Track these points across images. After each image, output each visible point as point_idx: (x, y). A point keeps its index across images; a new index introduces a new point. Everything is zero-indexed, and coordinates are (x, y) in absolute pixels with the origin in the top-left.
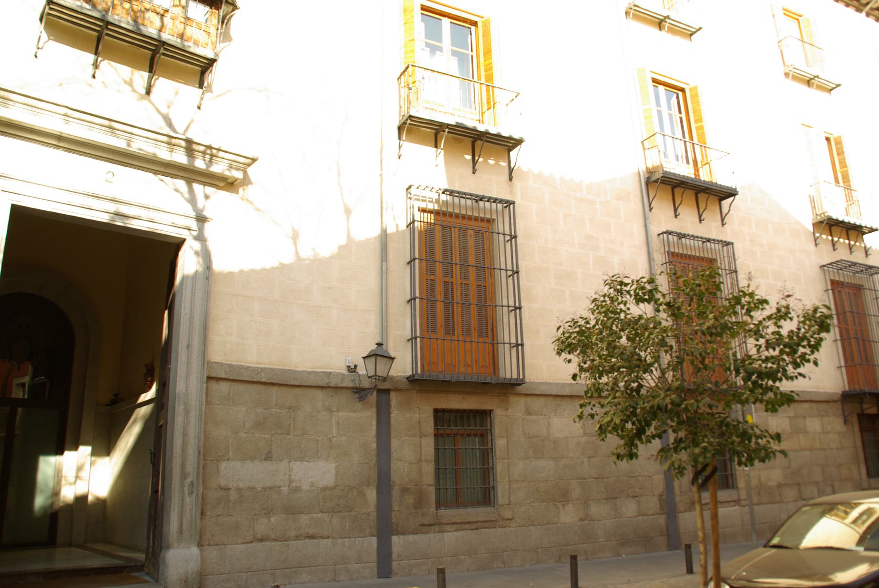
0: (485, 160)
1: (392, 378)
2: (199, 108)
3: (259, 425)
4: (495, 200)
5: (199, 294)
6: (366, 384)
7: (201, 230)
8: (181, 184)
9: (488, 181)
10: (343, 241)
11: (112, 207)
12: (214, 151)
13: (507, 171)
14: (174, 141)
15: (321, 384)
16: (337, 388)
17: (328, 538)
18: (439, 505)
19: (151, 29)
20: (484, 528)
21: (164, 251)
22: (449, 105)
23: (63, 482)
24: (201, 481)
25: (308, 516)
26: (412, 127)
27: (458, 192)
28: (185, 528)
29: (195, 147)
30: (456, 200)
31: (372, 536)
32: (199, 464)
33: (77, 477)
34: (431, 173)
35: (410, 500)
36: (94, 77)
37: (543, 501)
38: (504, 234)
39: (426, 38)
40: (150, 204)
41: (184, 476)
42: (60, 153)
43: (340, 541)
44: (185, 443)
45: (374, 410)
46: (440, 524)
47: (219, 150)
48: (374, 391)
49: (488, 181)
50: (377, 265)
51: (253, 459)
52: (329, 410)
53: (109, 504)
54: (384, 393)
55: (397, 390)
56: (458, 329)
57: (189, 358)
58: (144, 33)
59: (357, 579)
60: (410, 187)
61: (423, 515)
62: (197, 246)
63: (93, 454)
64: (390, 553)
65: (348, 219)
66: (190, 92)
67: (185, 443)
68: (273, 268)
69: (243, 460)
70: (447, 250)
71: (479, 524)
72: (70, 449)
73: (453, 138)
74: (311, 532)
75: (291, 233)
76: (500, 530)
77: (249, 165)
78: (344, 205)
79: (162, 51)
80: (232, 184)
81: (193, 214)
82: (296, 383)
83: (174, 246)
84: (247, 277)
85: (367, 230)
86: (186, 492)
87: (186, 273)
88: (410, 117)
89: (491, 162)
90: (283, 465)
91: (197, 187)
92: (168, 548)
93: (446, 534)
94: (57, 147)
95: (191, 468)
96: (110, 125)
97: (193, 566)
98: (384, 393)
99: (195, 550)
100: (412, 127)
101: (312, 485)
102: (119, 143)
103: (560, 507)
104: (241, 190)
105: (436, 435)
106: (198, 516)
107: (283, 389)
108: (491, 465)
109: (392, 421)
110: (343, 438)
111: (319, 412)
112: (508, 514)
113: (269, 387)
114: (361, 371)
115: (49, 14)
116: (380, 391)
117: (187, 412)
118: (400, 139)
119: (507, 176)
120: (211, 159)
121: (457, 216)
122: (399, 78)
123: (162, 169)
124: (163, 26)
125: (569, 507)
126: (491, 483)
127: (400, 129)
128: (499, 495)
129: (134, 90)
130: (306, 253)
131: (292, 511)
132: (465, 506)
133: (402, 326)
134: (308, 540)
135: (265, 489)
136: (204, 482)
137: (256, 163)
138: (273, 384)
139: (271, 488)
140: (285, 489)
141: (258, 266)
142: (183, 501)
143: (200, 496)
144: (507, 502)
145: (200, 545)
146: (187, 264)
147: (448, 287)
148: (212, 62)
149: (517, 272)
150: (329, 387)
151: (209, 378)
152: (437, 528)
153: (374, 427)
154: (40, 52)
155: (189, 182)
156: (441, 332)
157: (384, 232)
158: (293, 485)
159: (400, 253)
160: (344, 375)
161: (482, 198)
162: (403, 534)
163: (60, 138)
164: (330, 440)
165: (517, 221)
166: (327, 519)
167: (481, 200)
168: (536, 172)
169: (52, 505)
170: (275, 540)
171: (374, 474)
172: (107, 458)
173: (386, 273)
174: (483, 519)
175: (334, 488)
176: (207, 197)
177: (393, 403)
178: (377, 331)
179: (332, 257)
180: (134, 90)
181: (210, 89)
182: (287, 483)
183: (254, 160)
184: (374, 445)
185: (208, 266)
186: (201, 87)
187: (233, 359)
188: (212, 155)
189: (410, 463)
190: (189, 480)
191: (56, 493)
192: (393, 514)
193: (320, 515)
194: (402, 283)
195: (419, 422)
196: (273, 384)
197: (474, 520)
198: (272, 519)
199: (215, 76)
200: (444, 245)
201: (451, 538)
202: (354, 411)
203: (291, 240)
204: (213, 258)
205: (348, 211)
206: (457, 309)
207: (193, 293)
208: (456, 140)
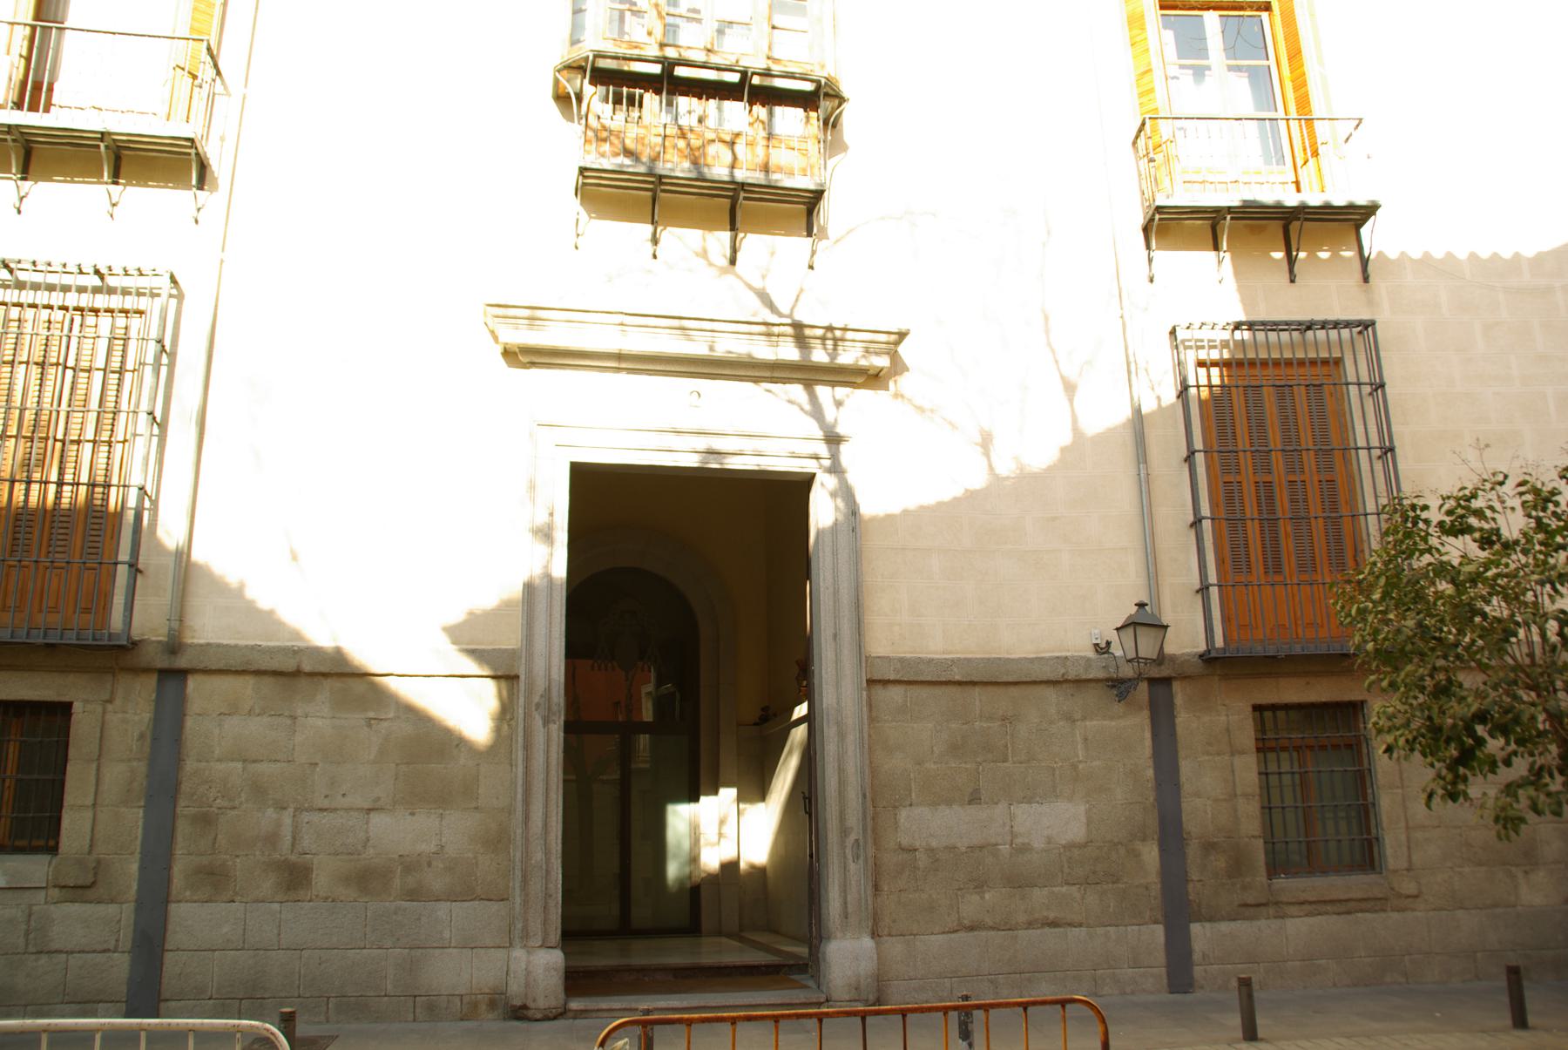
0: (1312, 254)
1: (1173, 658)
2: (811, 267)
3: (956, 748)
4: (1336, 325)
5: (844, 555)
6: (1128, 671)
7: (835, 457)
8: (797, 391)
9: (1323, 290)
10: (1066, 438)
11: (702, 443)
12: (838, 334)
13: (1357, 265)
14: (776, 330)
15: (1052, 677)
16: (1079, 682)
17: (1080, 925)
18: (1273, 870)
19: (719, 170)
20: (1362, 911)
21: (785, 495)
22: (1233, 166)
23: (702, 842)
24: (870, 841)
25: (1045, 891)
26: (1166, 225)
27: (1263, 323)
28: (850, 909)
29: (808, 332)
30: (1261, 336)
31: (1156, 922)
32: (864, 813)
33: (720, 835)
34: (1211, 296)
35: (1219, 862)
36: (655, 257)
37: (1480, 864)
38: (1359, 384)
39: (1228, 58)
40: (756, 430)
41: (844, 832)
42: (623, 377)
43: (1100, 931)
44: (842, 783)
45: (1146, 713)
46: (1276, 903)
47: (845, 329)
48: (1141, 681)
49: (1323, 290)
50: (1131, 470)
51: (949, 802)
52: (1071, 720)
53: (770, 872)
54: (1161, 684)
55: (1184, 678)
56: (1289, 563)
57: (838, 654)
58: (709, 176)
59: (1133, 993)
60: (1173, 332)
61: (1244, 888)
62: (831, 482)
63: (741, 798)
64: (1189, 952)
65: (1071, 401)
66: (796, 245)
67: (842, 783)
68: (955, 499)
69: (934, 804)
70: (1258, 426)
71: (1351, 905)
72: (707, 794)
73: (1246, 226)
74: (1052, 915)
75: (979, 440)
76: (1395, 915)
77: (897, 343)
78: (1062, 377)
79: (742, 195)
80: (877, 376)
81: (820, 434)
82: (1010, 679)
83: (800, 486)
84: (914, 519)
85: (1106, 412)
86: (850, 857)
87: (821, 526)
88: (1159, 209)
89: (1324, 255)
90: (1000, 810)
91: (823, 392)
92: (829, 938)
93: (1289, 922)
94: (619, 370)
95: (853, 820)
96: (680, 324)
97: (867, 966)
98: (1161, 684)
99: (867, 942)
100: (1166, 225)
101: (1049, 840)
102: (698, 348)
103: (1520, 875)
104: (891, 384)
105: (1258, 750)
106: (870, 891)
107: (991, 689)
108: (1370, 798)
109: (1179, 730)
110: (1097, 763)
111: (1052, 722)
112: (1409, 887)
113: (969, 689)
114: (1117, 651)
115: (584, 184)
116: (1152, 681)
117: (842, 736)
118: (1148, 247)
119: (1358, 275)
120: (835, 345)
121: (1264, 363)
122: (1134, 143)
123: (768, 374)
124: (735, 158)
125: (1540, 876)
126: (1374, 831)
127: (1146, 230)
128: (1389, 851)
129: (711, 264)
130: (1005, 468)
131: (1018, 882)
132: (1324, 872)
133: (1183, 567)
134: (1047, 930)
135: (972, 848)
136: (876, 842)
137: (907, 340)
138: (973, 683)
139: (981, 847)
140: (1005, 849)
141: (930, 500)
142: (845, 868)
143: (871, 862)
144: (1405, 865)
145: (875, 934)
146: (822, 512)
147: (1266, 492)
148: (818, 195)
149: (1392, 449)
150: (1067, 681)
151: (871, 682)
152: (1271, 911)
153: (1148, 742)
154: (580, 241)
155: (809, 385)
156: (1258, 568)
157: (1137, 411)
158: (1019, 841)
159: (1168, 447)
160: (1088, 660)
161: (1309, 326)
162: (1211, 919)
163: (619, 357)
164: (1074, 767)
165: (1382, 354)
166: (1077, 895)
167: (1309, 328)
168: (1416, 254)
169: (690, 877)
170: (992, 928)
171: (1153, 822)
172: (761, 805)
173: (1148, 482)
174: (1359, 895)
175: (1085, 845)
176: (839, 404)
177: (1179, 700)
178: (1141, 581)
179: (1049, 469)
180: (711, 264)
181: (823, 234)
182: (1008, 838)
183: (902, 335)
184: (1150, 773)
185: (853, 511)
186: (810, 234)
187: (906, 650)
188: (835, 340)
189: (1216, 800)
190: (852, 837)
191: (694, 859)
192: (1190, 886)
193: (1064, 889)
194: (1176, 497)
195: (1228, 730)
196: (973, 683)
197: (1342, 897)
198: (987, 896)
199: (829, 211)
200: (1285, 421)
201: (1298, 929)
202: (1112, 718)
203: (980, 449)
204: (859, 499)
205: (1070, 388)
206: (1285, 528)
207: (835, 553)
208: (1252, 229)
